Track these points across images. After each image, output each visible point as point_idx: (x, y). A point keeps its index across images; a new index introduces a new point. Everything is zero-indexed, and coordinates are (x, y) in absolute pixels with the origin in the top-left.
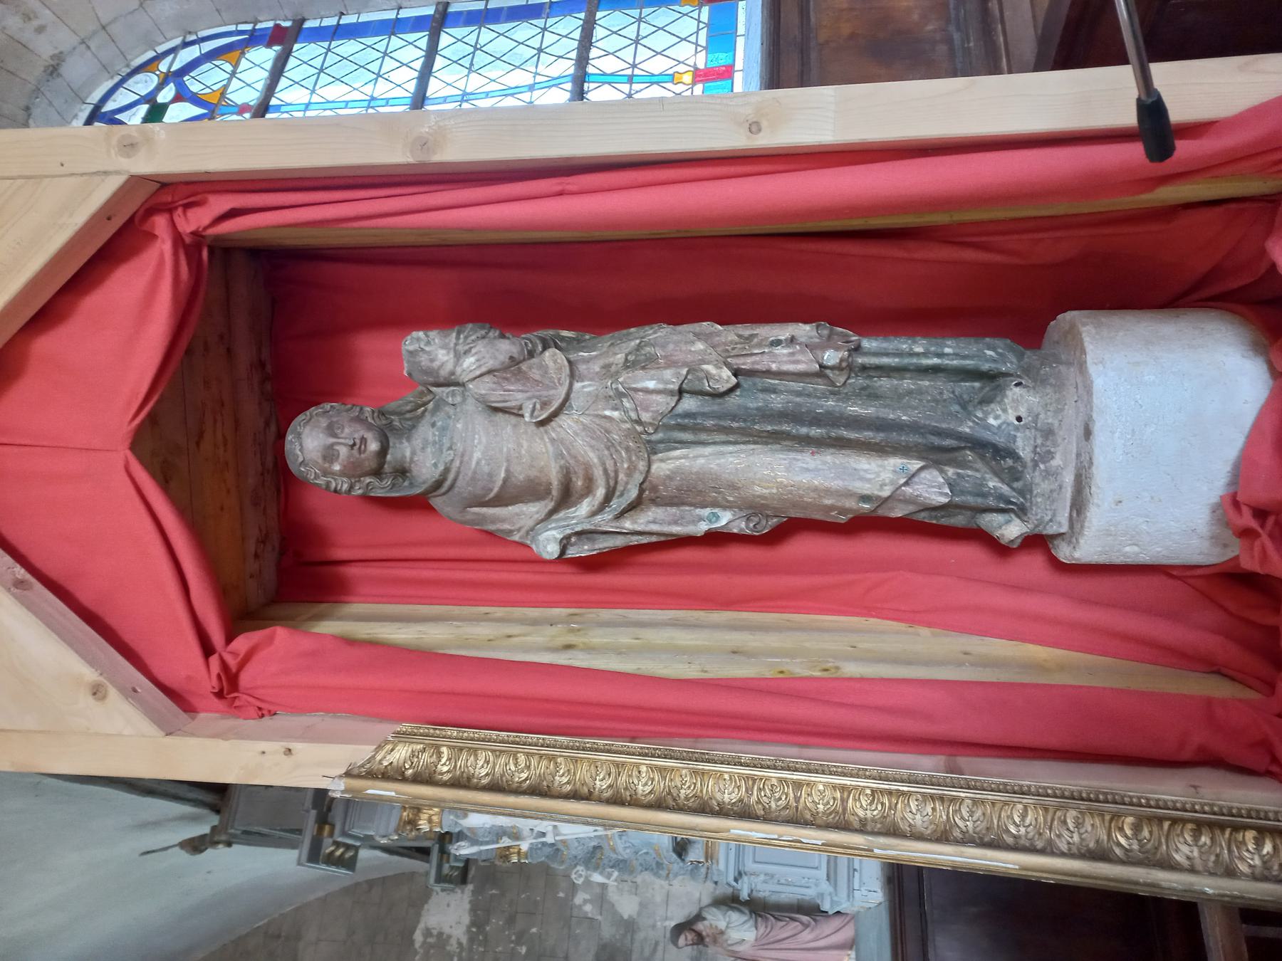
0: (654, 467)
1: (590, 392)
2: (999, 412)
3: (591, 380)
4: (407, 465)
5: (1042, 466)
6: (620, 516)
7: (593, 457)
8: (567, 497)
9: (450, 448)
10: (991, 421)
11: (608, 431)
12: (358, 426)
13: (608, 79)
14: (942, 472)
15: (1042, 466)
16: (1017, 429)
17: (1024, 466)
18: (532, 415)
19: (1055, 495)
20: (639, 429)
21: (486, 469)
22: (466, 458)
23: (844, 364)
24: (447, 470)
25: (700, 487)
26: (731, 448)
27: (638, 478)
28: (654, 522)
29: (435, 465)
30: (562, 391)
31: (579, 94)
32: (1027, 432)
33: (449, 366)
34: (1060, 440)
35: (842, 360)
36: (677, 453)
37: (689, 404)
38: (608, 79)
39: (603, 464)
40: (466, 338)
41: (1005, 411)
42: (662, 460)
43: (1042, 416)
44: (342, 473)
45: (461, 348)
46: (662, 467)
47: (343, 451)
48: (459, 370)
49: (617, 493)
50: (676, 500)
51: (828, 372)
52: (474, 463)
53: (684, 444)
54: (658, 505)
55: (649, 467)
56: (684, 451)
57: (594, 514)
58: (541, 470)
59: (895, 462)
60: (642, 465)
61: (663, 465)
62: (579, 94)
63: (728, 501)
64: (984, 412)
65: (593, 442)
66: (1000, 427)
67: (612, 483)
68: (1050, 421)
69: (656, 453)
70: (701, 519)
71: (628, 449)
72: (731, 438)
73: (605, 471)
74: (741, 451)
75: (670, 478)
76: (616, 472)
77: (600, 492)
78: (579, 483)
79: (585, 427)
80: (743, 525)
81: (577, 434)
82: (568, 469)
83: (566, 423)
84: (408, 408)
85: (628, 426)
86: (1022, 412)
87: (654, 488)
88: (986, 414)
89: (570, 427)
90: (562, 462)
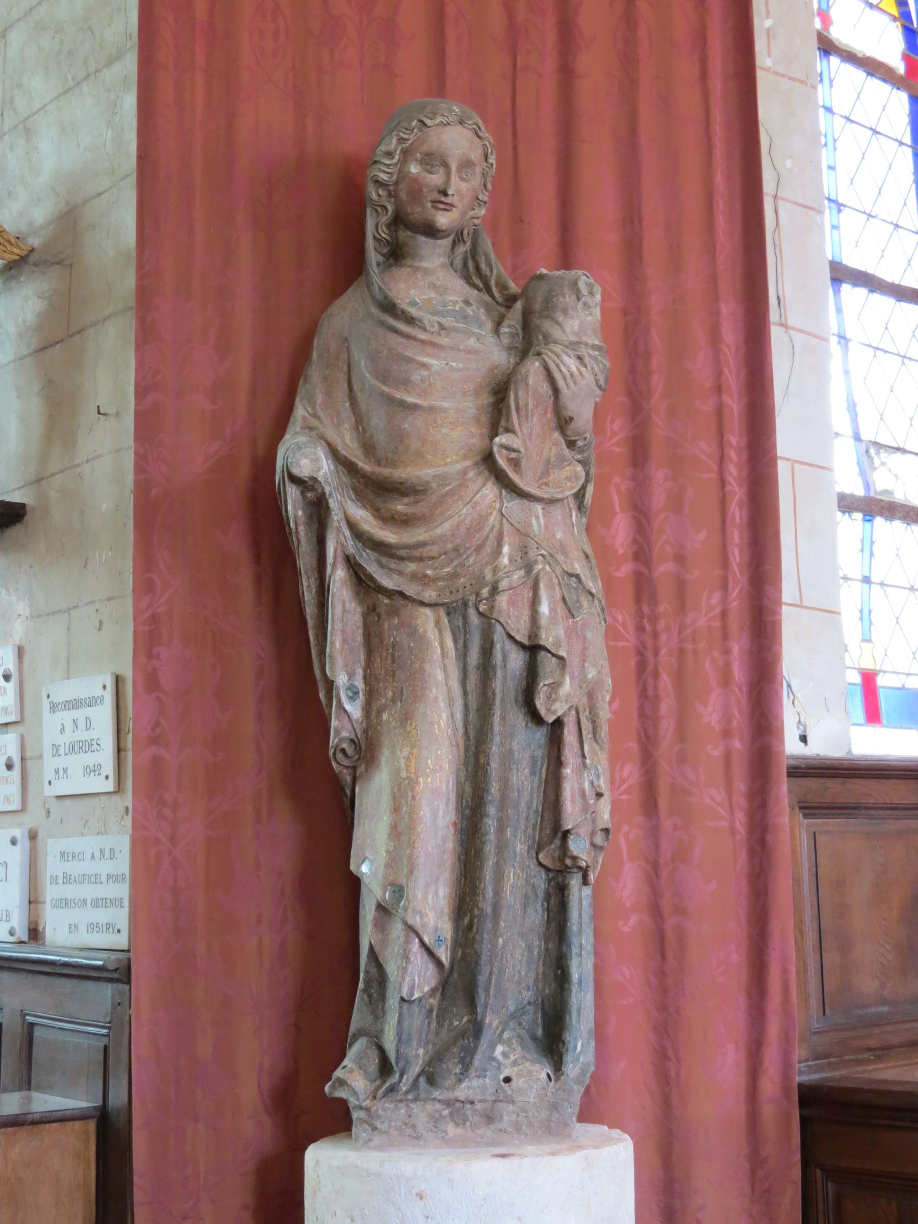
0: (428, 611)
1: (531, 525)
2: (512, 1057)
3: (546, 527)
4: (409, 261)
5: (446, 1112)
6: (352, 564)
7: (444, 528)
8: (376, 489)
9: (442, 327)
10: (499, 1049)
11: (479, 548)
12: (467, 200)
13: (868, 547)
14: (433, 991)
15: (446, 1112)
16: (496, 1078)
17: (451, 1089)
18: (503, 446)
19: (409, 1131)
20: (485, 592)
21: (416, 377)
22: (429, 349)
23: (568, 862)
24: (410, 320)
25: (401, 675)
26: (459, 716)
27: (411, 590)
28: (344, 611)
29: (414, 303)
30: (533, 490)
31: (847, 504)
32: (491, 1090)
33: (556, 333)
34: (480, 1132)
35: (574, 858)
36: (450, 643)
37: (516, 660)
38: (868, 547)
39: (433, 543)
40: (595, 358)
41: (515, 1063)
42: (437, 623)
43: (511, 1107)
44: (403, 176)
45: (583, 351)
46: (429, 624)
47: (436, 179)
48: (558, 349)
49: (384, 560)
50: (375, 641)
51: (557, 842)
52: (425, 360)
53: (463, 655)
54: (365, 616)
55: (429, 605)
56: (452, 653)
57: (352, 526)
58: (419, 454)
59: (447, 929)
60: (430, 595)
61: (431, 624)
62: (847, 504)
63: (379, 712)
64: (510, 1039)
65: (463, 529)
66: (493, 1059)
67: (403, 553)
68: (505, 1118)
69: (448, 614)
70: (351, 676)
71: (454, 576)
72: (472, 716)
73: (423, 544)
74: (455, 728)
75: (413, 633)
76: (420, 559)
77: (389, 536)
78: (400, 507)
79: (484, 518)
80: (345, 734)
81: (474, 507)
82: (424, 492)
83: (489, 491)
84: (483, 266)
85: (489, 576)
86: (517, 1083)
87: (393, 612)
88: (508, 1043)
89: (484, 497)
90: (434, 485)
